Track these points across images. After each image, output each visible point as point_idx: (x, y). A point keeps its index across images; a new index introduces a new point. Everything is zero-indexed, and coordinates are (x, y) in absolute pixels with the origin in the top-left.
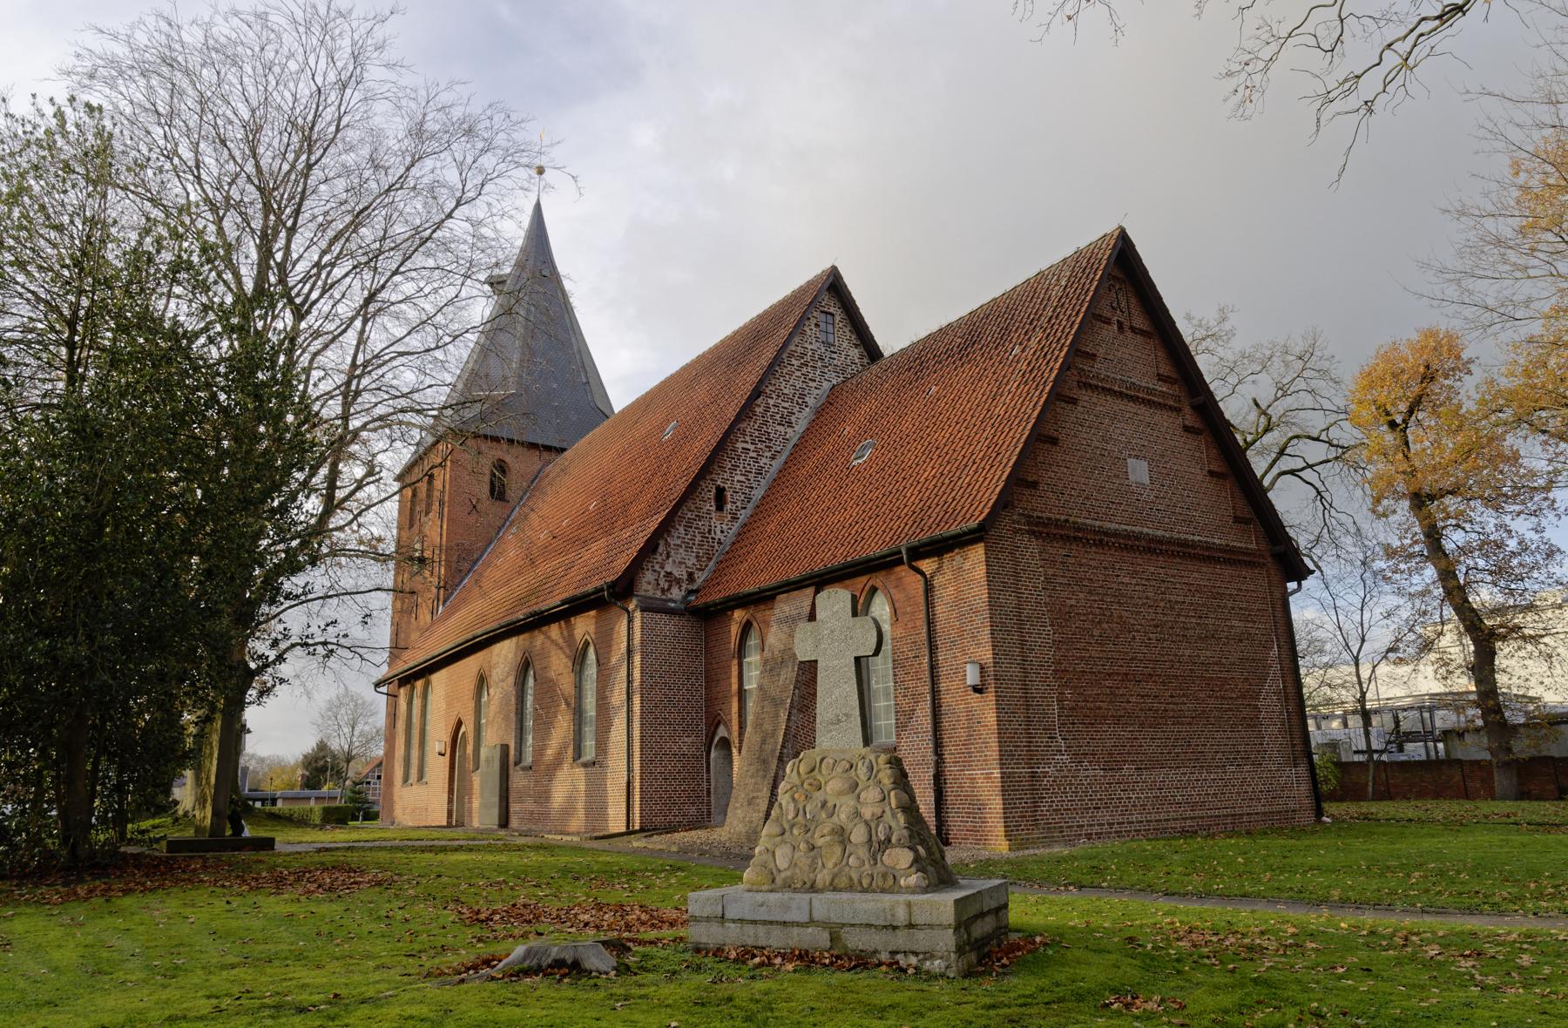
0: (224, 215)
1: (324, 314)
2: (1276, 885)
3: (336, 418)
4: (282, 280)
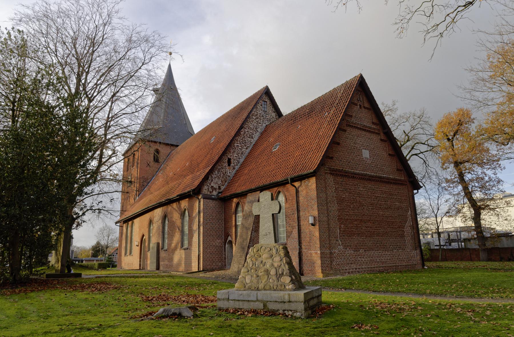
0: (65, 67)
2: (409, 288)
4: (84, 89)
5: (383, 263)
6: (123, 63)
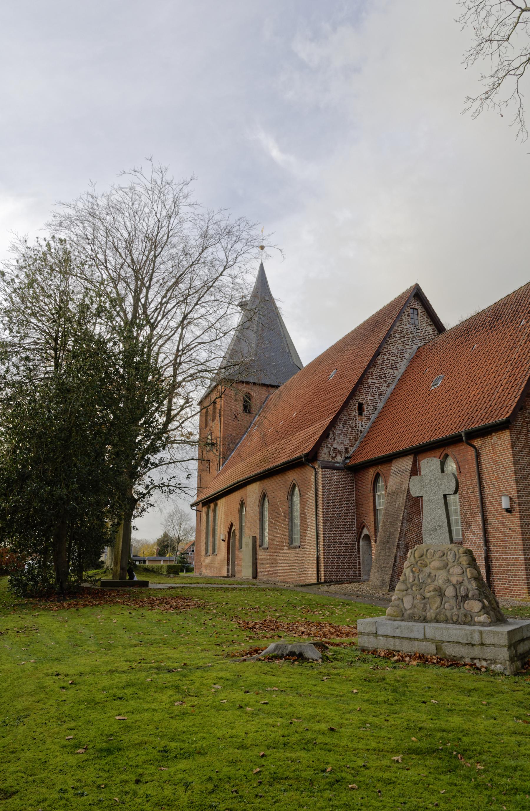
0: (118, 283)
1: (164, 326)
3: (171, 376)
4: (145, 312)
6: (195, 269)
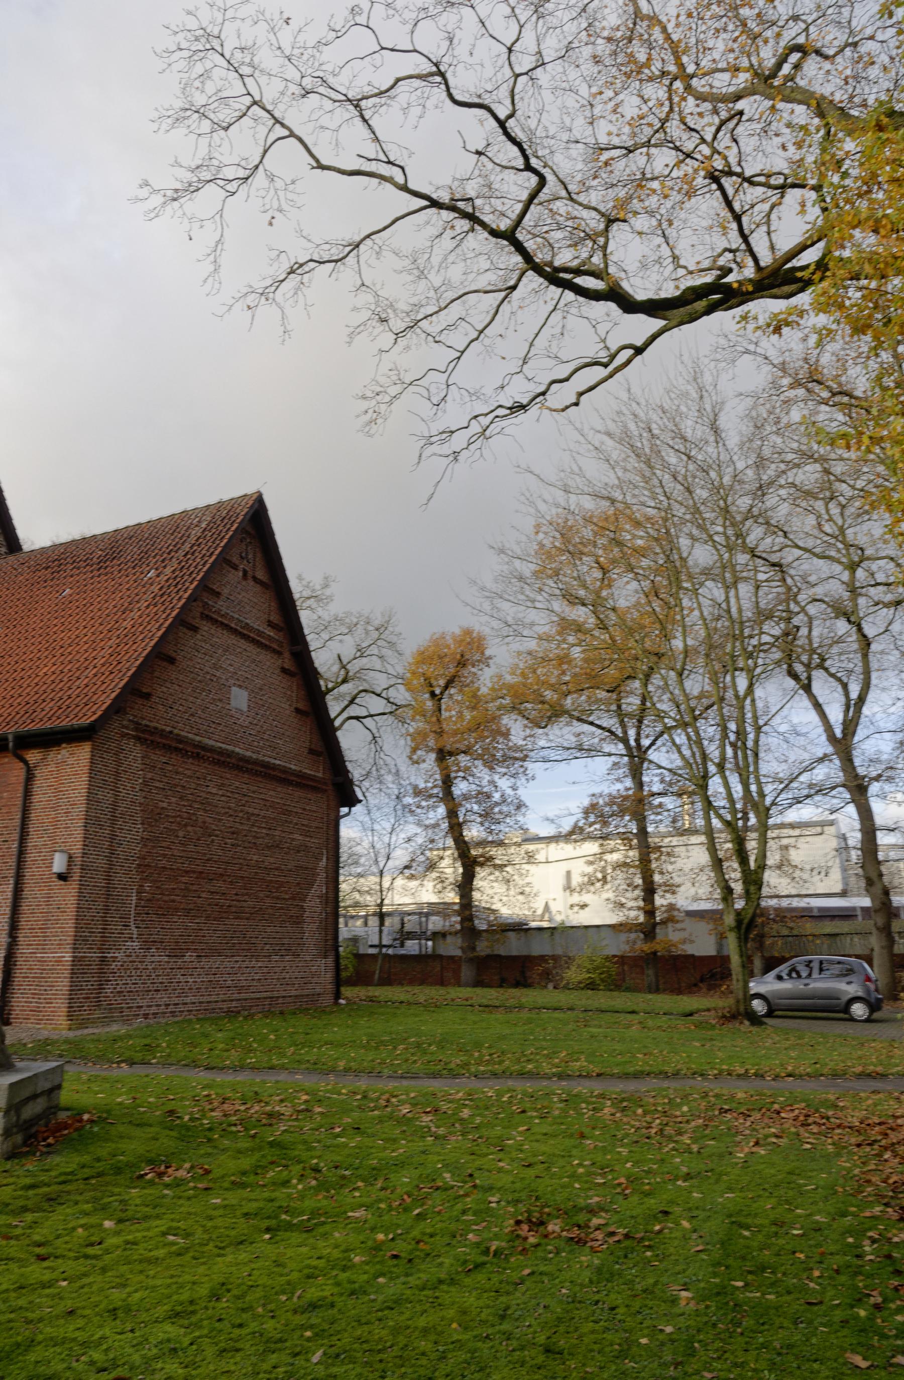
5: (240, 989)
